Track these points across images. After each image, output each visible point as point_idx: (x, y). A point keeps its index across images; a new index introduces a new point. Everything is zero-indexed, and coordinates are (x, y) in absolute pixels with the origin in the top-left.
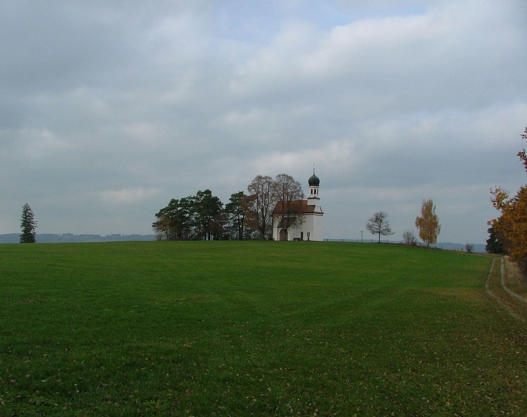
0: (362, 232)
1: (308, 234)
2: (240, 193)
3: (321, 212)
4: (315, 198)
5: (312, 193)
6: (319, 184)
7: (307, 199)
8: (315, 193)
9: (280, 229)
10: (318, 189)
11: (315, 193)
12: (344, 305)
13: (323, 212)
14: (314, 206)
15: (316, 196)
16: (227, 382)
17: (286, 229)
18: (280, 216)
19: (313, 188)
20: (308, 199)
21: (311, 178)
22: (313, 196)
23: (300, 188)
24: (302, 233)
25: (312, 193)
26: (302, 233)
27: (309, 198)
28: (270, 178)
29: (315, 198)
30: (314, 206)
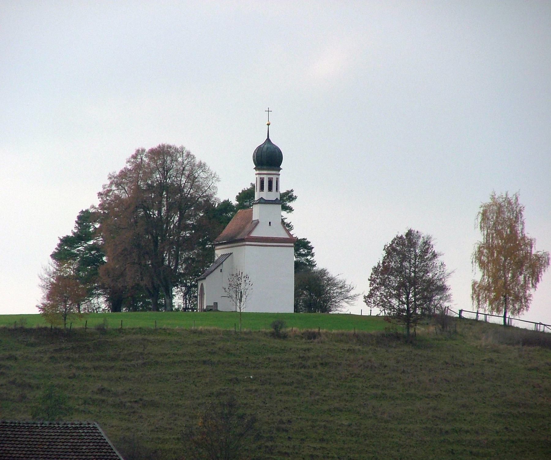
5: (262, 189)
8: (270, 189)
10: (277, 176)
11: (270, 189)
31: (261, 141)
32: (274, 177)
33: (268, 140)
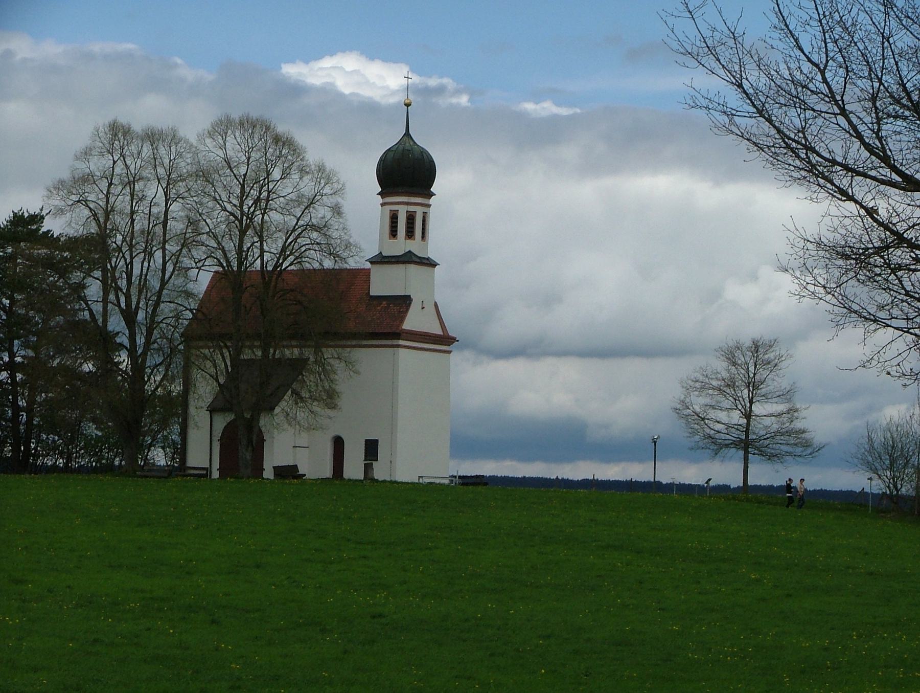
0: (805, 199)
1: (371, 449)
2: (18, 220)
3: (440, 332)
4: (408, 259)
5: (394, 233)
6: (431, 188)
7: (368, 265)
8: (410, 233)
9: (221, 422)
10: (425, 209)
11: (410, 233)
12: (94, 243)
13: (451, 334)
14: (404, 301)
15: (414, 246)
16: (544, 670)
17: (255, 419)
18: (221, 349)
19: (403, 205)
20: (373, 261)
21: (391, 154)
22: (400, 246)
23: (337, 210)
24: (338, 443)
25: (394, 233)
26: (338, 443)
27: (380, 260)
28: (174, 139)
29: (408, 259)
30: (404, 301)
31: (390, 138)
32: (419, 210)
33: (407, 134)
